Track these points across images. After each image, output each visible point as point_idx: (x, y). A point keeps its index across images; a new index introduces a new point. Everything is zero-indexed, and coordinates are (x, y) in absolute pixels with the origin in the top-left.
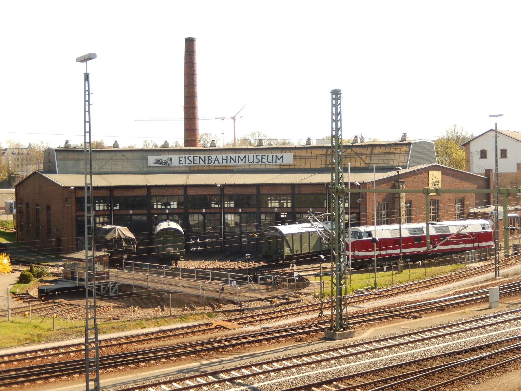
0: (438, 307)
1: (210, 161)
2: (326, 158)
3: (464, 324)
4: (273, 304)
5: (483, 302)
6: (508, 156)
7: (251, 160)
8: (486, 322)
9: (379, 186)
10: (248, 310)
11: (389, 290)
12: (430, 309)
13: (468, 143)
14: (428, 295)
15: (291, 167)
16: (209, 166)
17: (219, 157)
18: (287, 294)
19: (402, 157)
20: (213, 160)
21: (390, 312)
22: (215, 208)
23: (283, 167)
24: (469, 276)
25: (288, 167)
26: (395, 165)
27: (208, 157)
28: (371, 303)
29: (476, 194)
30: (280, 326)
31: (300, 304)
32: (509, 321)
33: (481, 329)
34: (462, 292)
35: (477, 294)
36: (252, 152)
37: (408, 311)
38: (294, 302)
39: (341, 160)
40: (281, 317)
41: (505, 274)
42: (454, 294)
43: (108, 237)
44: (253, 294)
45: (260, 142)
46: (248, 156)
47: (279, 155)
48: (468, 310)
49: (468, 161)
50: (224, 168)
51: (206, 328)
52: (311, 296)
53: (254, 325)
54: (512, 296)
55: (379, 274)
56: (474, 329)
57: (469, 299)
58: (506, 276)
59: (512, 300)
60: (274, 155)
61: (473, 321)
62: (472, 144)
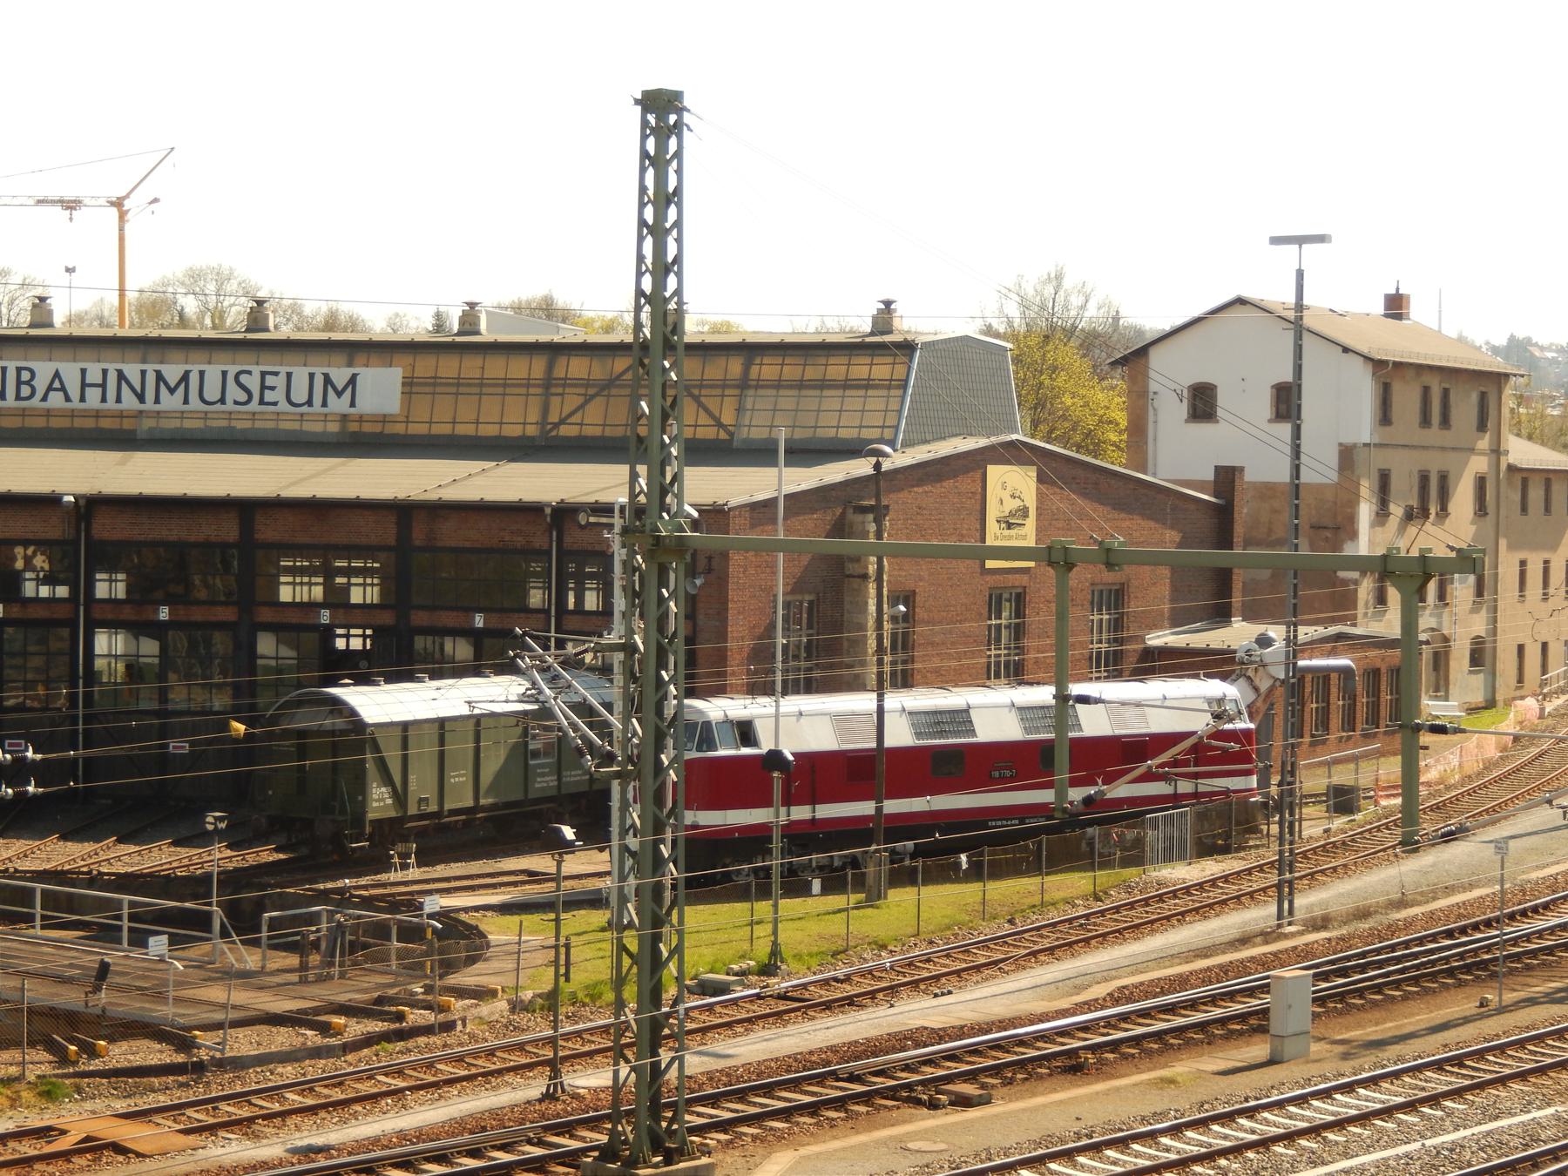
0: (1055, 1055)
1: (25, 391)
2: (547, 395)
3: (1176, 1131)
4: (333, 1041)
5: (1241, 1033)
6: (1394, 419)
7: (212, 393)
8: (1267, 1122)
9: (759, 529)
10: (222, 1064)
11: (836, 980)
12: (1021, 1064)
13: (1143, 352)
14: (1005, 1000)
15: (392, 429)
16: (23, 413)
17: (70, 372)
18: (391, 992)
19: (876, 400)
20: (41, 384)
21: (853, 1078)
22: (37, 600)
23: (353, 427)
24: (1168, 918)
25: (377, 428)
26: (867, 434)
27: (19, 370)
28: (766, 1034)
29: (1174, 571)
30: (375, 1142)
31: (456, 1042)
32: (1363, 1118)
33: (1250, 1155)
34: (1147, 990)
35: (1214, 1000)
36: (219, 355)
37: (930, 1072)
38: (427, 1030)
39: (673, 405)
40: (374, 1098)
41: (1318, 913)
42: (1115, 999)
43: (283, 840)
44: (230, 987)
45: (257, 314)
46: (202, 373)
47: (340, 375)
48: (1182, 1067)
49: (1138, 429)
50: (89, 423)
51: (33, 1153)
52: (501, 1005)
53: (256, 1136)
54: (1359, 1008)
55: (789, 906)
56: (1224, 1153)
57: (1179, 1021)
58: (1322, 923)
59: (1359, 1026)
60: (319, 372)
61: (1216, 1119)
62: (1156, 358)
